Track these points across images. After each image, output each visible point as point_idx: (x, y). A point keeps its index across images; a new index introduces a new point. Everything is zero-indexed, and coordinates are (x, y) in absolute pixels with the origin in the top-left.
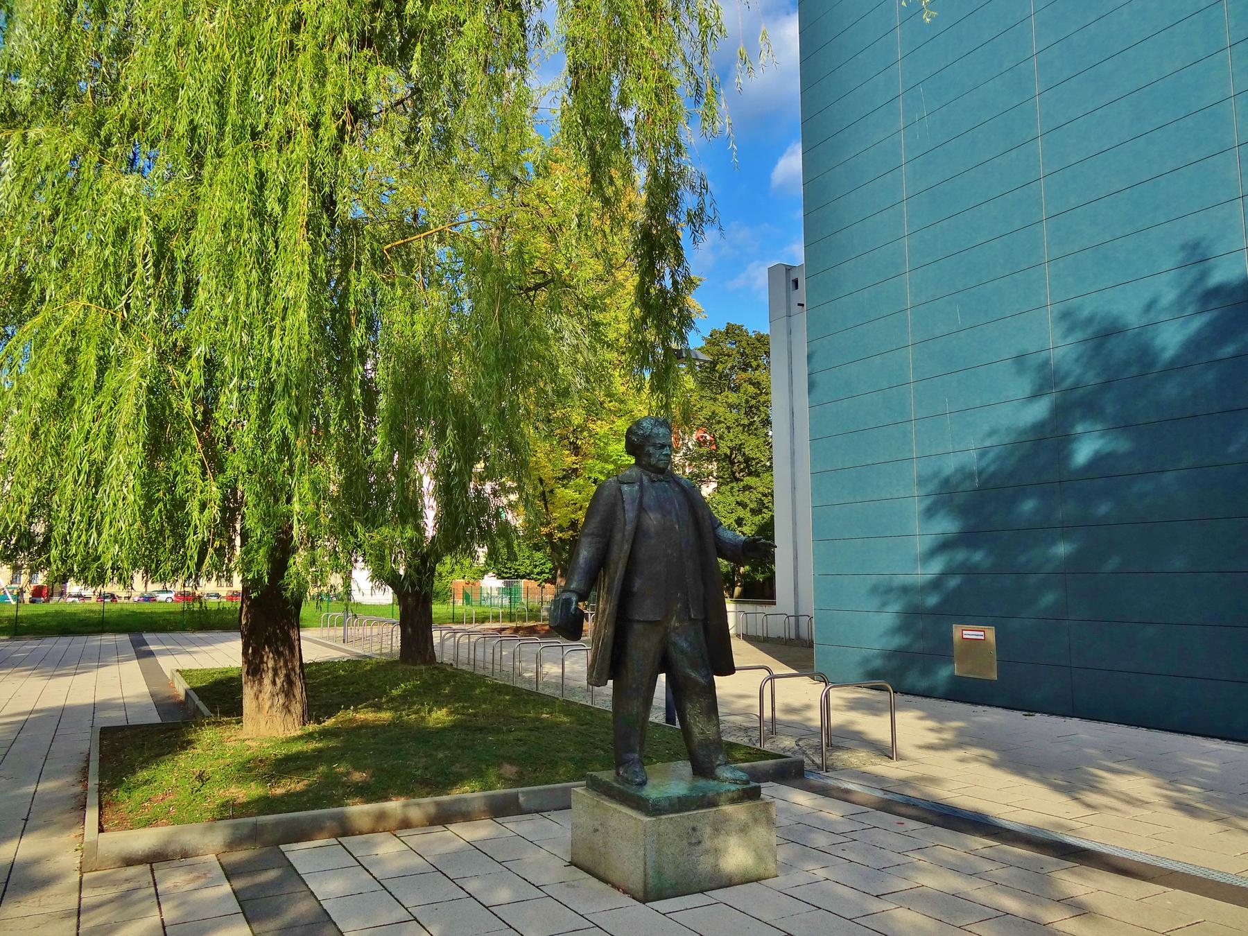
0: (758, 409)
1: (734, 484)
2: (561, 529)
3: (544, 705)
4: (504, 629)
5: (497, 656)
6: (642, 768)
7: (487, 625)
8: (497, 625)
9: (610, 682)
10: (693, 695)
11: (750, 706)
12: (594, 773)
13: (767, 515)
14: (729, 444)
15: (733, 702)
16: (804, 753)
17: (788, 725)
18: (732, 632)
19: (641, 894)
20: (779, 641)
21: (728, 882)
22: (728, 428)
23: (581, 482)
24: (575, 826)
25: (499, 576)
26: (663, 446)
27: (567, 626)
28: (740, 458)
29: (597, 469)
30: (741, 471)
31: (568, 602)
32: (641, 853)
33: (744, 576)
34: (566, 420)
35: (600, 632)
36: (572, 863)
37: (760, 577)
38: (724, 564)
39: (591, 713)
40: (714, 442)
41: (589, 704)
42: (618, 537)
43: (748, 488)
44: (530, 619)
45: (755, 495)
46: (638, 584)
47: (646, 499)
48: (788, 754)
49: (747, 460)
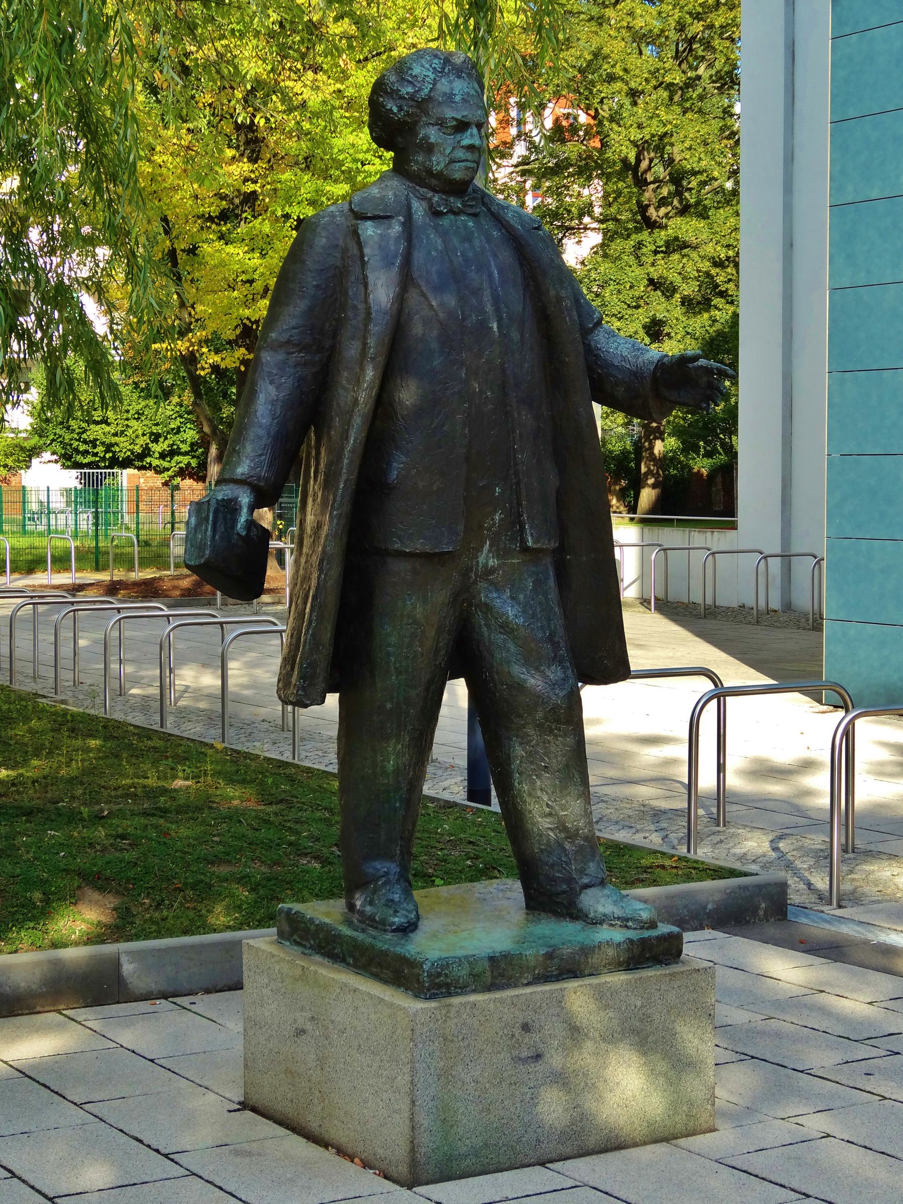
1: (645, 236)
2: (215, 343)
4: (81, 587)
5: (66, 650)
6: (407, 893)
7: (40, 578)
8: (64, 579)
9: (332, 700)
10: (526, 730)
11: (671, 762)
12: (297, 907)
13: (722, 314)
14: (635, 134)
15: (626, 754)
16: (789, 866)
17: (759, 806)
18: (629, 592)
19: (403, 1170)
21: (613, 1144)
22: (634, 94)
23: (267, 228)
24: (251, 1024)
25: (68, 460)
26: (462, 126)
27: (231, 568)
28: (660, 171)
29: (308, 194)
30: (663, 202)
31: (229, 508)
32: (403, 1080)
33: (664, 462)
34: (224, 72)
35: (306, 579)
36: (244, 1106)
37: (702, 465)
38: (609, 425)
39: (291, 779)
40: (598, 129)
41: (287, 757)
42: (351, 350)
43: (676, 246)
44: (145, 563)
45: (695, 264)
46: (398, 467)
47: (418, 257)
48: (753, 868)
49: (677, 178)
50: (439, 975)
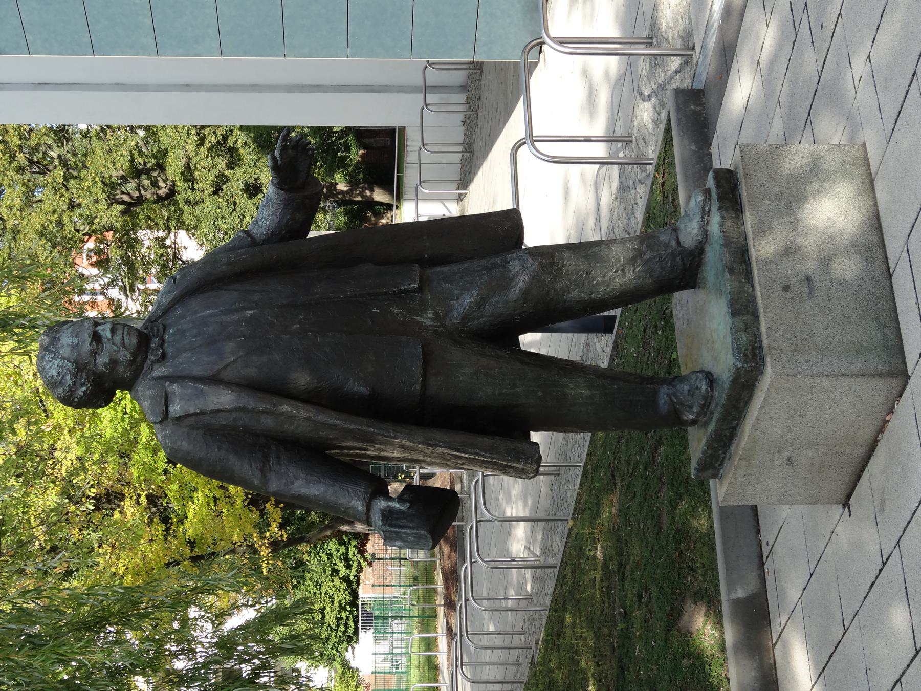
0: (35, 149)
1: (180, 198)
2: (262, 526)
3: (581, 551)
4: (449, 629)
5: (497, 640)
6: (683, 379)
7: (443, 660)
8: (443, 642)
9: (535, 437)
10: (560, 288)
12: (694, 464)
13: (240, 138)
14: (103, 205)
16: (662, 87)
18: (453, 210)
19: (895, 383)
20: (471, 124)
21: (875, 222)
22: (72, 206)
23: (175, 487)
24: (783, 499)
25: (351, 639)
26: (97, 338)
27: (434, 516)
28: (131, 186)
29: (149, 456)
30: (155, 184)
31: (389, 516)
32: (826, 383)
33: (353, 183)
36: (846, 504)
37: (356, 154)
38: (324, 226)
39: (596, 469)
40: (98, 233)
41: (579, 471)
42: (268, 422)
43: (188, 173)
44: (430, 580)
45: (202, 159)
46: (357, 387)
47: (196, 371)
48: (664, 114)
49: (136, 172)
50: (746, 355)
